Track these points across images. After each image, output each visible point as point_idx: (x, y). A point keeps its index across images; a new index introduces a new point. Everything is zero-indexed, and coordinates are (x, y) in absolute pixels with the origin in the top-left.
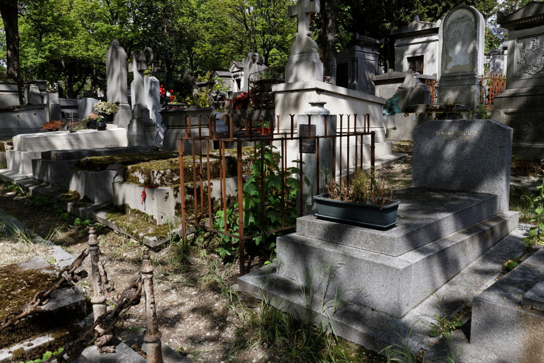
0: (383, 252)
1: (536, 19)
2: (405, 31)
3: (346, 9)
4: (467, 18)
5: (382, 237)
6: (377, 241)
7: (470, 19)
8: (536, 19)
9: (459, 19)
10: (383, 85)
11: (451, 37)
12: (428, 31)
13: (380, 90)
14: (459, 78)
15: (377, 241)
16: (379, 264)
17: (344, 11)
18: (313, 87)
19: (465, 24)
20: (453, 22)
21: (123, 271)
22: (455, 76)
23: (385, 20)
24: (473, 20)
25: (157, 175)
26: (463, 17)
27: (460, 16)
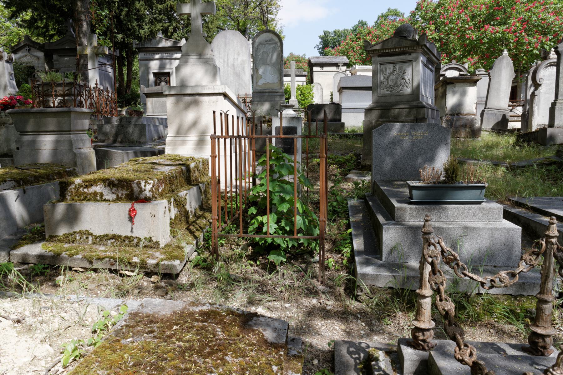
0: (491, 220)
1: (397, 50)
2: (149, 46)
3: (103, 14)
4: (273, 42)
5: (490, 208)
6: (485, 213)
7: (276, 43)
8: (397, 50)
9: (266, 41)
10: (156, 99)
11: (260, 57)
12: (171, 49)
13: (152, 104)
14: (267, 94)
15: (485, 213)
16: (501, 229)
17: (101, 15)
18: (221, 92)
19: (272, 46)
20: (260, 44)
21: (115, 324)
22: (263, 93)
23: (116, 31)
24: (279, 44)
25: (145, 186)
26: (270, 41)
27: (268, 39)
